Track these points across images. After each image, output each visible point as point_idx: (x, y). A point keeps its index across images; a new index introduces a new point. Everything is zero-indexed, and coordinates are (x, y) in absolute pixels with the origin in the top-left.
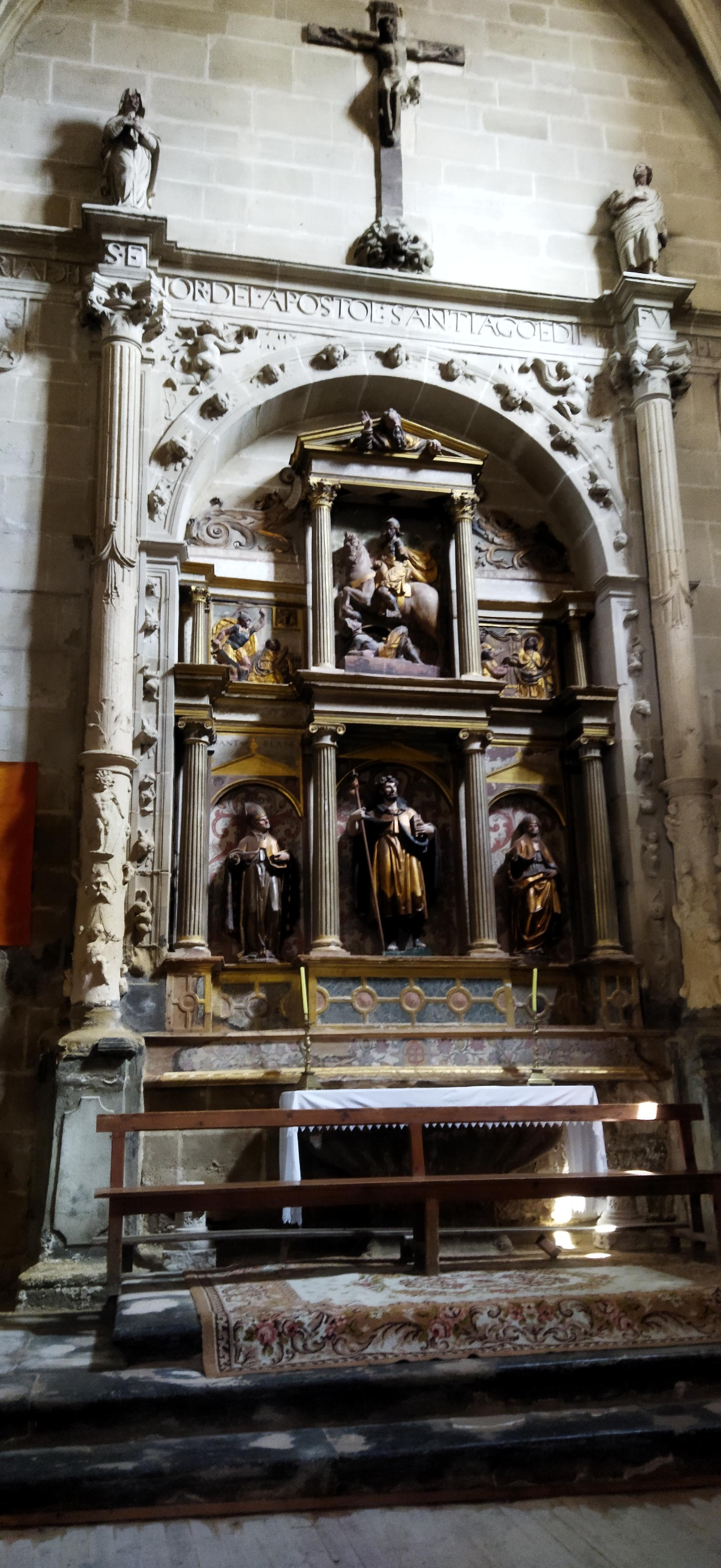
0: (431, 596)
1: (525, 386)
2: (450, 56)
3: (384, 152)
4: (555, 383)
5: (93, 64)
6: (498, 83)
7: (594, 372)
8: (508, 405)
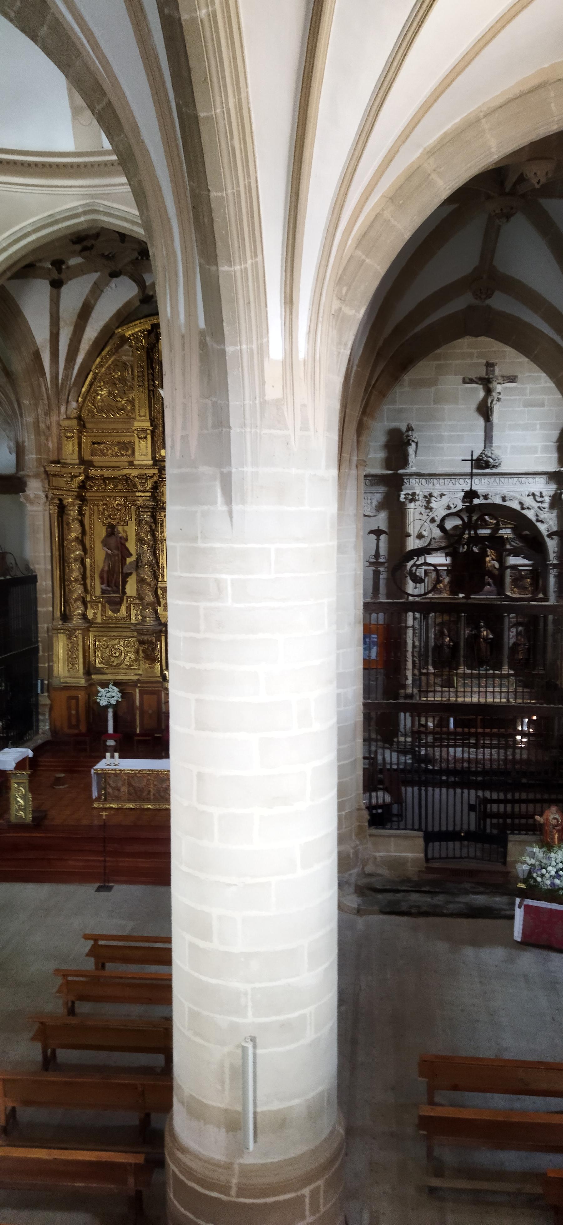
0: (497, 565)
1: (529, 501)
2: (512, 379)
3: (488, 424)
4: (539, 499)
5: (398, 406)
6: (529, 387)
7: (552, 493)
8: (523, 508)
